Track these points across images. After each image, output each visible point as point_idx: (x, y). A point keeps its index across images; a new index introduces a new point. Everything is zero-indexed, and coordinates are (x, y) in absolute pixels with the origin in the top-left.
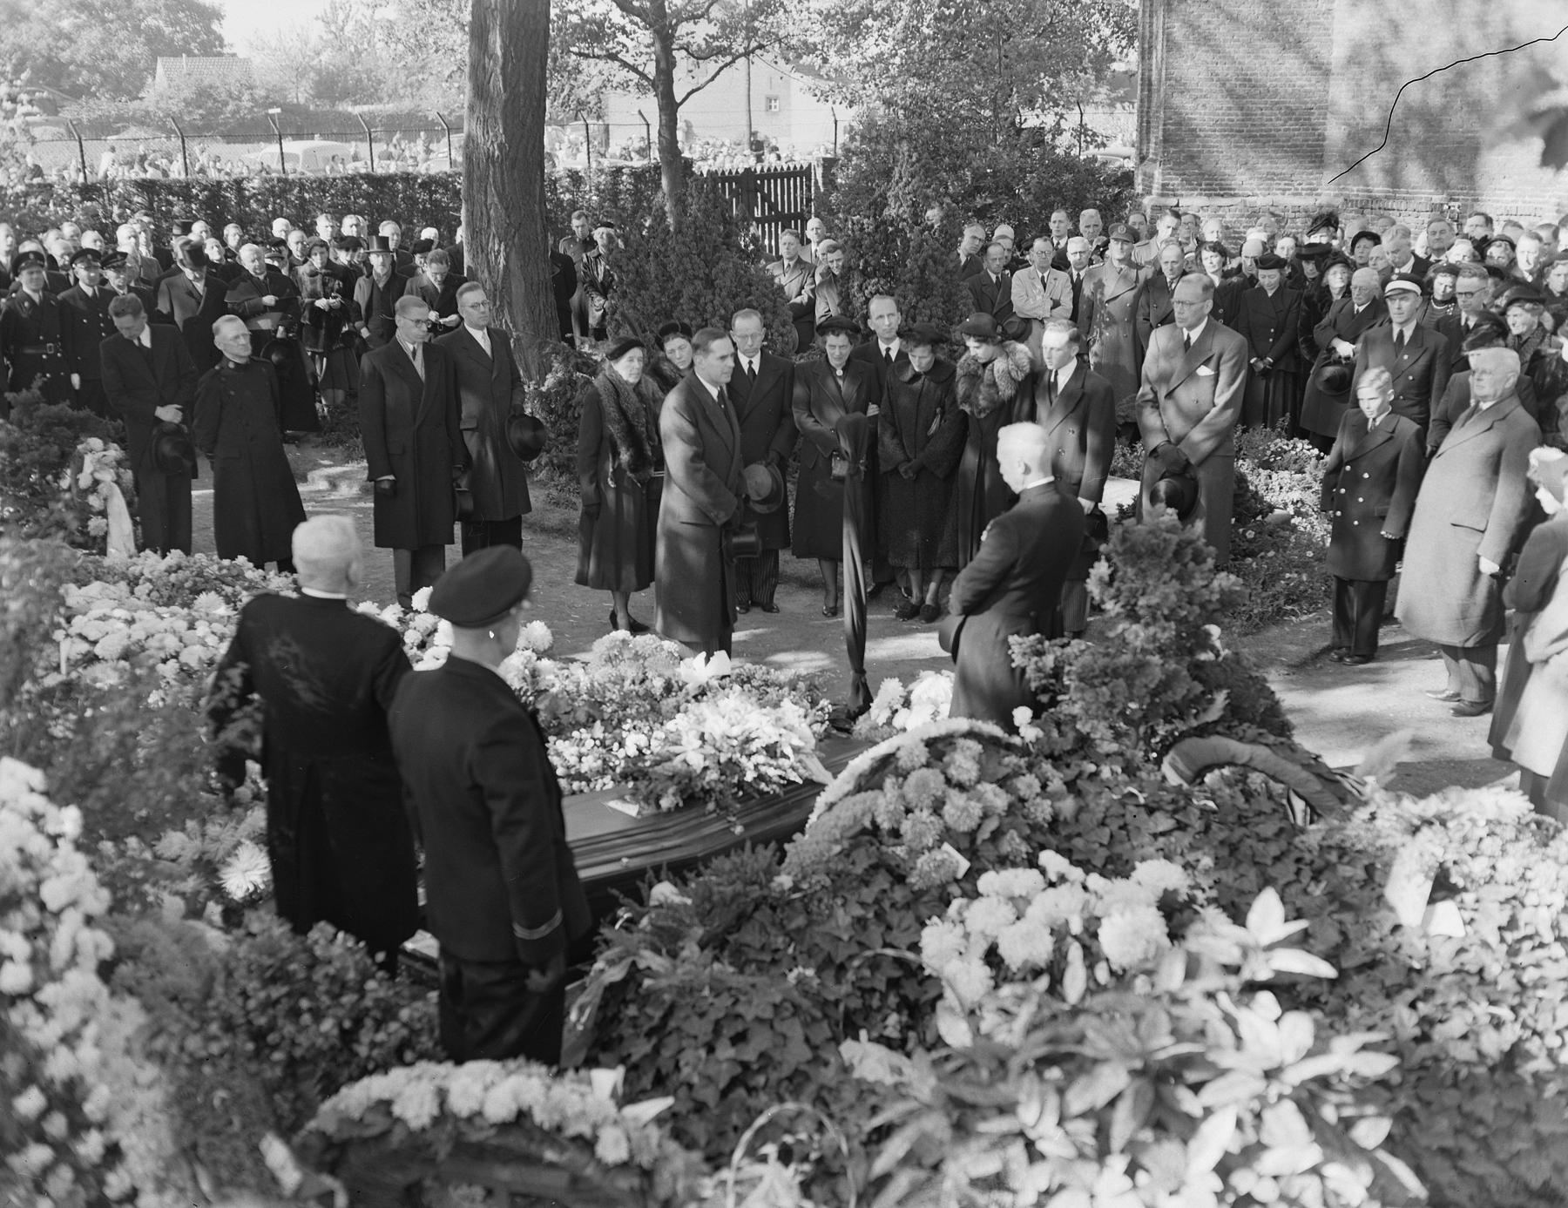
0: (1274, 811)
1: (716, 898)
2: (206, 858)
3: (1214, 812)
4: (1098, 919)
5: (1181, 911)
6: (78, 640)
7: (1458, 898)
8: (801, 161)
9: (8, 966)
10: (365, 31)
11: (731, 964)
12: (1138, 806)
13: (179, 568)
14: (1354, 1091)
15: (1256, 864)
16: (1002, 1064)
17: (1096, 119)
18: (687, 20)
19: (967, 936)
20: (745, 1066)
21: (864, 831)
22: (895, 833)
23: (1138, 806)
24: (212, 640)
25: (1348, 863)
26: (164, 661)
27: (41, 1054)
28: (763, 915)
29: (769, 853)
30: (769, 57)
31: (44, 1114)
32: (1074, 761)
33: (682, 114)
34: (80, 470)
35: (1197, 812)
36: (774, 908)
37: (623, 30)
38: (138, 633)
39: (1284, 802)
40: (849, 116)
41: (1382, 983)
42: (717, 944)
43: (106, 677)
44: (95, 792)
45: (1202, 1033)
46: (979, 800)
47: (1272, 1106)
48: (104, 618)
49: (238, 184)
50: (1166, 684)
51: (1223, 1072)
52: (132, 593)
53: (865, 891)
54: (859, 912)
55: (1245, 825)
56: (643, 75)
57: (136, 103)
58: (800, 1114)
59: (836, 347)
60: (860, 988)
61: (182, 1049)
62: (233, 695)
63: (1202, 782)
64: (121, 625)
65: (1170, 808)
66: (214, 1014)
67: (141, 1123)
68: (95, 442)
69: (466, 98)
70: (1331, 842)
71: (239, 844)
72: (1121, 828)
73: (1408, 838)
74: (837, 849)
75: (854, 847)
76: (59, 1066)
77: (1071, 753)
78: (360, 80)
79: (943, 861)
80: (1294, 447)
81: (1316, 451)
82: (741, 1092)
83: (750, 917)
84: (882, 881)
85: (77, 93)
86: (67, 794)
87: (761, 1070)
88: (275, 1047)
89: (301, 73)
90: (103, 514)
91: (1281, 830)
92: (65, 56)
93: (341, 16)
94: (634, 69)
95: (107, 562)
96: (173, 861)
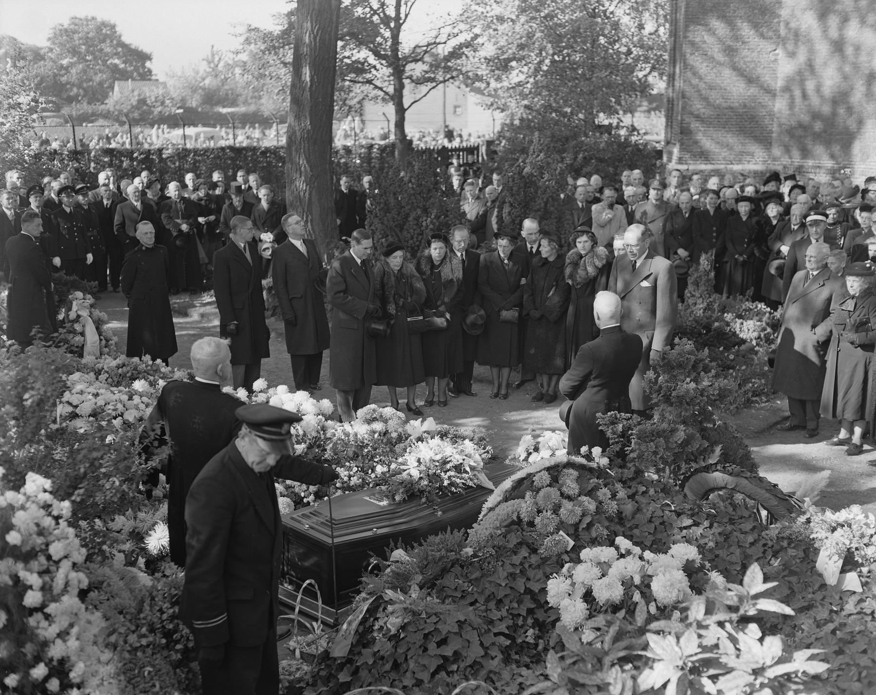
0: (750, 516)
1: (430, 558)
2: (137, 531)
3: (715, 516)
4: (651, 577)
5: (696, 573)
6: (66, 405)
7: (858, 570)
8: (473, 141)
9: (30, 593)
10: (230, 67)
11: (437, 598)
12: (671, 511)
13: (124, 365)
14: (804, 683)
15: (740, 546)
16: (600, 661)
17: (640, 120)
18: (411, 62)
19: (573, 584)
20: (445, 658)
21: (513, 523)
22: (531, 524)
23: (671, 511)
24: (142, 406)
25: (793, 548)
26: (115, 418)
27: (45, 644)
28: (457, 569)
29: (461, 534)
30: (457, 83)
31: (47, 679)
32: (633, 484)
33: (407, 114)
34: (70, 309)
35: (705, 516)
36: (462, 567)
37: (374, 67)
38: (100, 401)
39: (755, 511)
40: (500, 118)
41: (815, 618)
42: (428, 586)
43: (82, 426)
44: (76, 492)
45: (717, 646)
46: (580, 506)
47: (758, 691)
48: (82, 393)
49: (160, 151)
50: (687, 442)
51: (730, 671)
52: (97, 379)
53: (514, 557)
54: (511, 570)
55: (733, 524)
56: (386, 93)
57: (103, 106)
58: (478, 687)
59: (503, 246)
60: (511, 614)
61: (126, 642)
62: (156, 439)
63: (707, 499)
64: (90, 397)
65: (689, 513)
66: (144, 621)
67: (102, 684)
68: (79, 294)
69: (287, 103)
70: (784, 535)
71: (155, 523)
72: (661, 524)
73: (829, 534)
74: (499, 532)
75: (508, 532)
76: (56, 651)
77: (631, 479)
78: (227, 94)
79: (559, 541)
80: (756, 307)
81: (769, 309)
82: (443, 674)
83: (449, 571)
84: (524, 552)
85: (70, 100)
86: (62, 493)
87: (455, 661)
88: (177, 642)
89: (194, 90)
90: (82, 334)
91: (754, 528)
92: (64, 79)
93: (217, 59)
94: (381, 89)
95: (84, 361)
96: (118, 532)
